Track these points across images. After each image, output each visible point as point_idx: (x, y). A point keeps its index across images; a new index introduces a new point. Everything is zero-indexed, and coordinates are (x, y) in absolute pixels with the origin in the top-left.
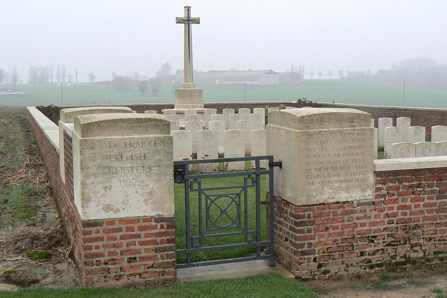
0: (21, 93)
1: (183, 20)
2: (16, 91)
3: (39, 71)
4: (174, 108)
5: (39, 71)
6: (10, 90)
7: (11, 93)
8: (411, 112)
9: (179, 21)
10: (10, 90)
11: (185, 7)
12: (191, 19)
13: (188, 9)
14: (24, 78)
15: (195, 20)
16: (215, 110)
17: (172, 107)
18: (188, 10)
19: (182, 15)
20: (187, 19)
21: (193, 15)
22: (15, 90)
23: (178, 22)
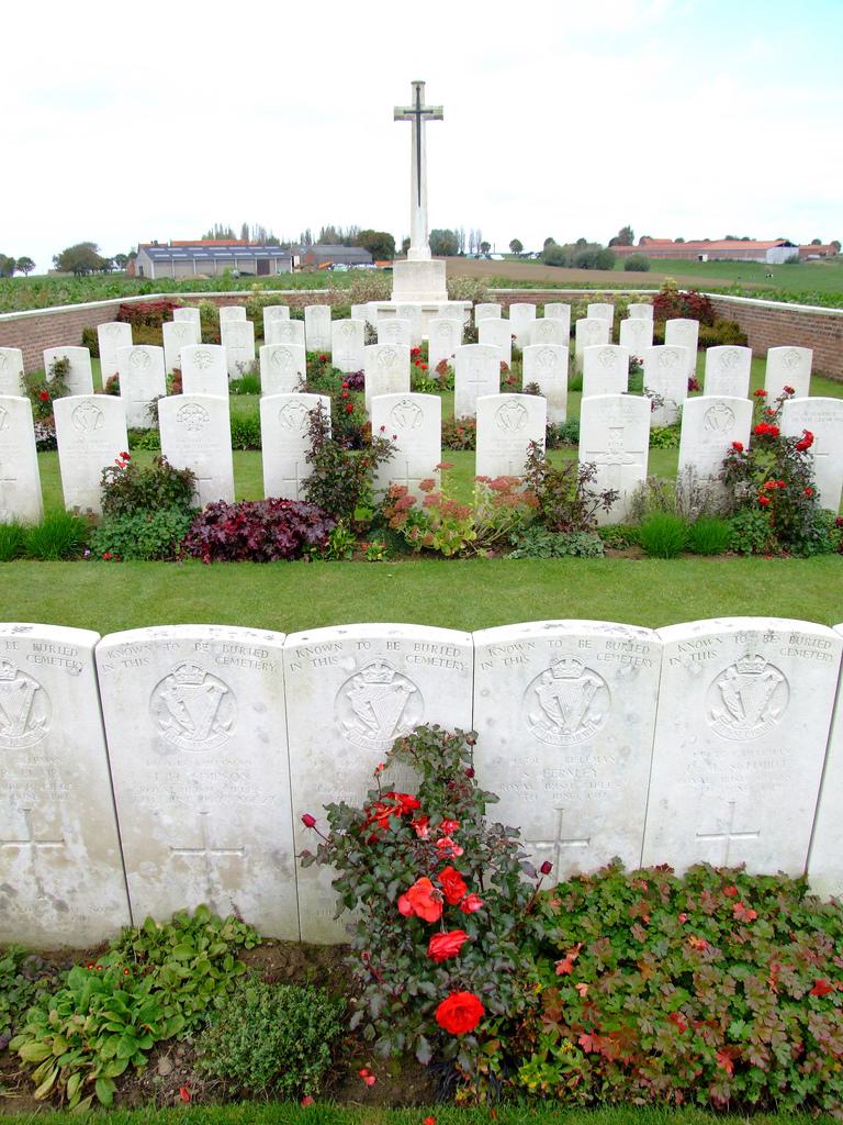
1: (405, 112)
11: (413, 83)
15: (431, 112)
18: (418, 89)
20: (414, 109)
23: (397, 118)
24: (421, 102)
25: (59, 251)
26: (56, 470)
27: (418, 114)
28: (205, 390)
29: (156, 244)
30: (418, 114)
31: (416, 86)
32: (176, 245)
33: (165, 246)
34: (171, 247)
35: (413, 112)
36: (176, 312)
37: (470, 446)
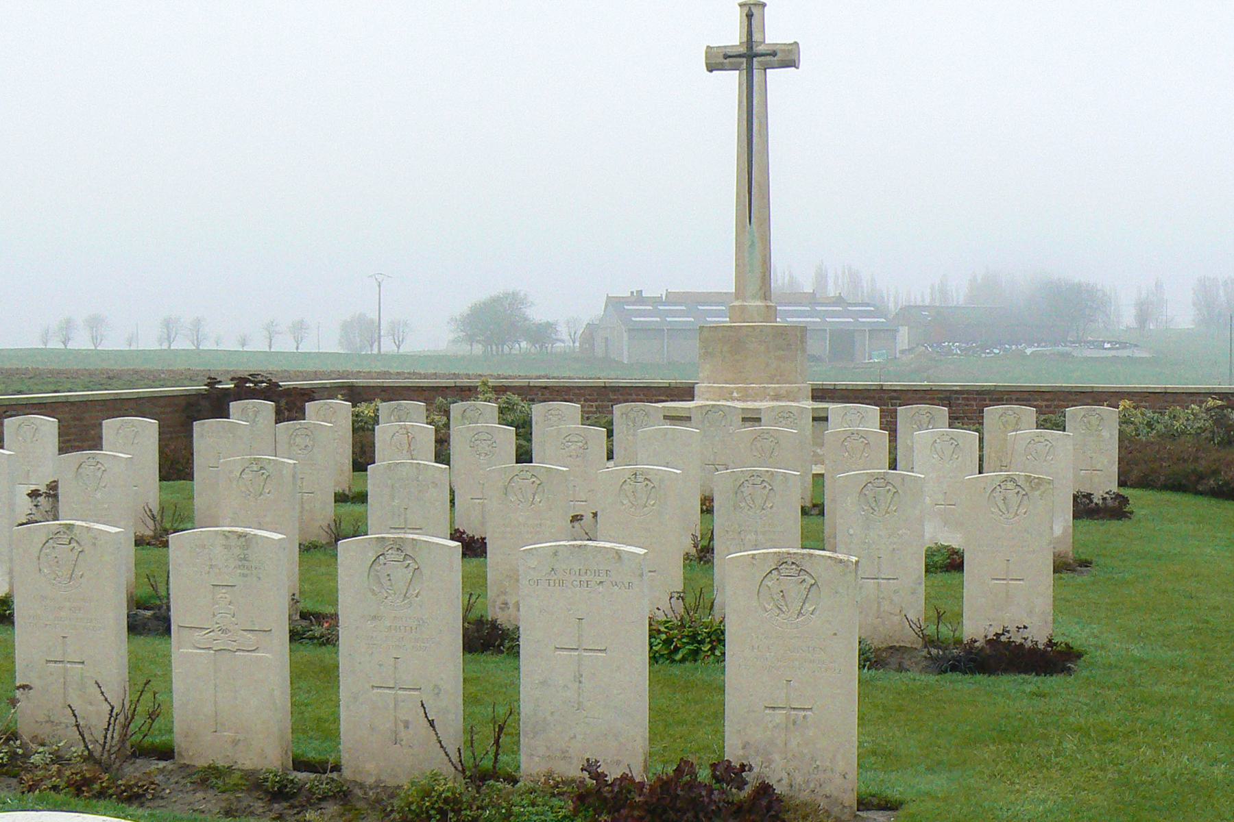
0: (1138, 354)
1: (726, 57)
2: (1125, 348)
3: (1221, 292)
4: (691, 397)
5: (1221, 292)
6: (1107, 346)
7: (1111, 354)
8: (86, 444)
9: (718, 61)
10: (1107, 346)
11: (741, 5)
12: (760, 49)
13: (751, 15)
14: (1181, 315)
15: (774, 54)
16: (1029, 413)
17: (687, 393)
18: (750, 16)
19: (732, 37)
20: (743, 50)
21: (774, 34)
22: (1124, 346)
23: (711, 68)
24: (756, 37)
25: (462, 307)
26: (330, 675)
27: (751, 59)
28: (555, 554)
29: (639, 298)
30: (751, 59)
31: (746, 10)
32: (673, 298)
33: (657, 301)
34: (665, 304)
35: (740, 56)
36: (309, 406)
37: (329, 641)
